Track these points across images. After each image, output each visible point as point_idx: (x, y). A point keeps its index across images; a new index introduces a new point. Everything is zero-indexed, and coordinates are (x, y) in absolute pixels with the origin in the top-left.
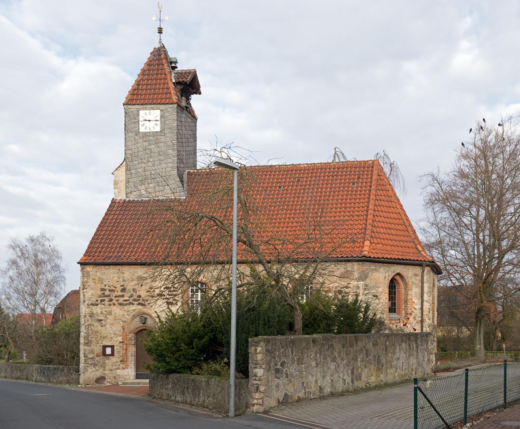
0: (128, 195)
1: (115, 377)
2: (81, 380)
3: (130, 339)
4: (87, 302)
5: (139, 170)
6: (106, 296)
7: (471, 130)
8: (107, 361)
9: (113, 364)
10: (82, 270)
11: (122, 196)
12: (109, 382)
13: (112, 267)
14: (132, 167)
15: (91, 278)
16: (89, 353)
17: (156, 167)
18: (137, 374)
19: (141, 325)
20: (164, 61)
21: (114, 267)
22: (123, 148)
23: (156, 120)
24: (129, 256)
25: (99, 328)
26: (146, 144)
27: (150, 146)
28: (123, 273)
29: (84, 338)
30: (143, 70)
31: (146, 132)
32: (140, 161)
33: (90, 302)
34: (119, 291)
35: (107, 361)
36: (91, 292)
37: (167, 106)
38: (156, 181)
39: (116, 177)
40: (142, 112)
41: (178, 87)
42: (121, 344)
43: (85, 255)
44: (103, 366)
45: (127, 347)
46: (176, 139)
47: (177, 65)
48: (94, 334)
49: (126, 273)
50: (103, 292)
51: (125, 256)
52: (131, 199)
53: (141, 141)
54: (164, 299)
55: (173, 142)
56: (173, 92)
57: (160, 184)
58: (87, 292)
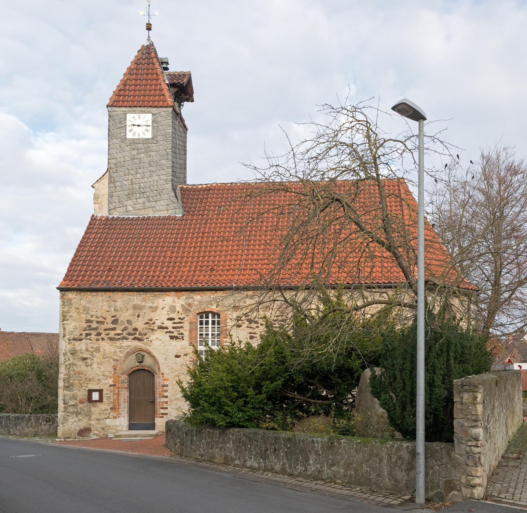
0: (111, 212)
1: (103, 429)
2: (60, 433)
3: (123, 382)
4: (68, 337)
5: (125, 182)
6: (92, 329)
7: (446, 165)
8: (93, 409)
9: (102, 412)
10: (62, 297)
11: (104, 213)
12: (96, 434)
13: (100, 293)
14: (116, 179)
15: (73, 307)
16: (70, 399)
17: (145, 179)
18: (130, 424)
19: (137, 364)
20: (155, 60)
21: (103, 293)
22: (107, 156)
23: (148, 126)
24: (122, 281)
25: (84, 368)
26: (135, 152)
27: (140, 155)
28: (115, 301)
29: (64, 380)
30: (130, 69)
31: (134, 139)
32: (127, 172)
33: (72, 337)
34: (110, 322)
35: (93, 409)
36: (74, 324)
37: (160, 109)
38: (145, 196)
39: (96, 190)
40: (129, 116)
41: (172, 89)
42: (112, 388)
43: (65, 280)
44: (88, 415)
45: (118, 391)
46: (171, 147)
47: (169, 66)
48: (77, 375)
49: (119, 300)
50: (88, 324)
51: (116, 281)
52: (115, 216)
53: (128, 149)
54: (167, 332)
55: (168, 151)
56: (167, 94)
57: (151, 199)
58: (68, 324)
